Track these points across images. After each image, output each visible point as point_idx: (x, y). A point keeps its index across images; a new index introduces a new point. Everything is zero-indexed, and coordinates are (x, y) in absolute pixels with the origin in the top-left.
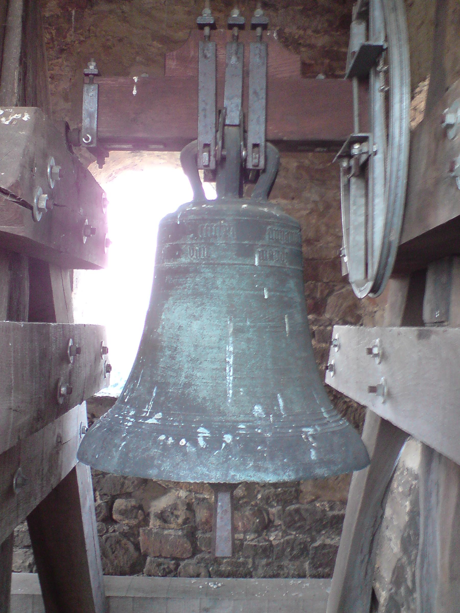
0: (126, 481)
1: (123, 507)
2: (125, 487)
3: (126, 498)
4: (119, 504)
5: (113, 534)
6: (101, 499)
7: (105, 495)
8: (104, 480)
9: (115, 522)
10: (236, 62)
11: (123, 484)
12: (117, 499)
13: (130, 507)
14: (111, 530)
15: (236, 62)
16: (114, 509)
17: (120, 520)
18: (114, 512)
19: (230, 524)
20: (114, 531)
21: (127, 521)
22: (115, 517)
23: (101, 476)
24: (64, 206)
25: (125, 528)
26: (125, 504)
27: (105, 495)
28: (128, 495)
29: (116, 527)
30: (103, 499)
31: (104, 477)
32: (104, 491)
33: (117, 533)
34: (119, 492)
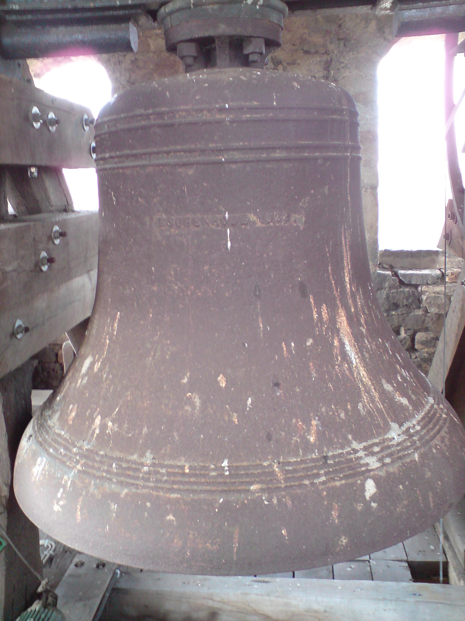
0: (427, 318)
1: (424, 339)
2: (426, 322)
3: (425, 331)
4: (419, 336)
5: (415, 360)
6: (405, 333)
7: (409, 329)
8: (408, 318)
9: (416, 350)
10: (176, 54)
11: (424, 321)
12: (417, 332)
13: (429, 338)
14: (413, 357)
15: (176, 54)
16: (416, 340)
17: (421, 349)
18: (416, 343)
19: (123, 564)
20: (416, 358)
21: (426, 350)
22: (416, 347)
23: (406, 315)
24: (26, 587)
25: (425, 355)
26: (425, 336)
27: (409, 329)
28: (426, 330)
29: (417, 354)
30: (408, 332)
31: (408, 315)
32: (409, 326)
33: (419, 359)
34: (420, 327)
